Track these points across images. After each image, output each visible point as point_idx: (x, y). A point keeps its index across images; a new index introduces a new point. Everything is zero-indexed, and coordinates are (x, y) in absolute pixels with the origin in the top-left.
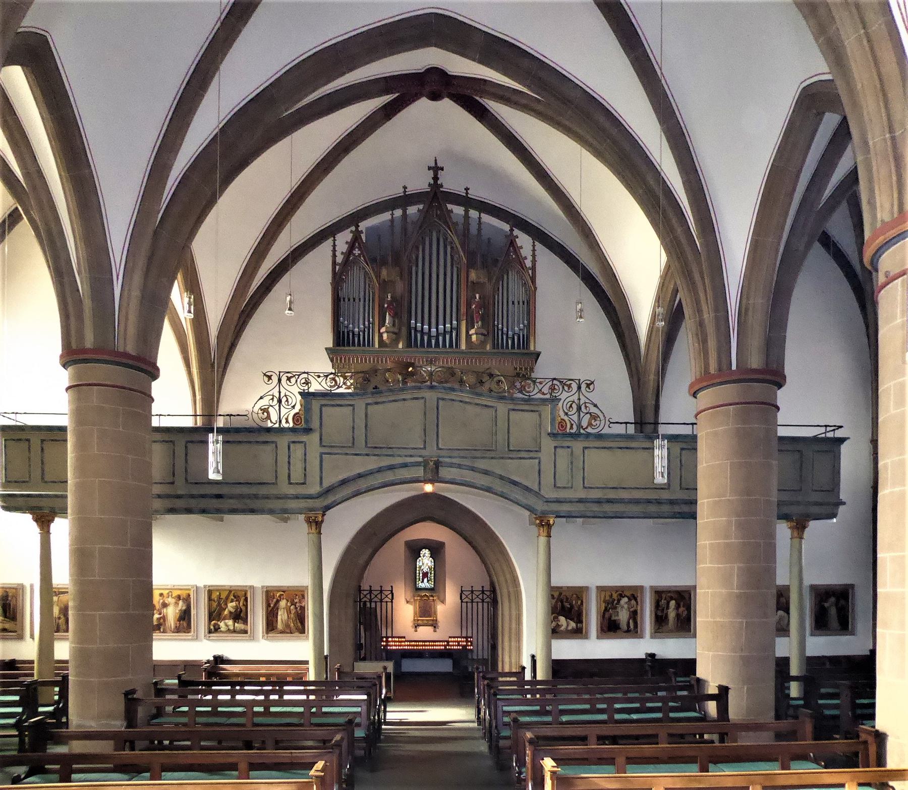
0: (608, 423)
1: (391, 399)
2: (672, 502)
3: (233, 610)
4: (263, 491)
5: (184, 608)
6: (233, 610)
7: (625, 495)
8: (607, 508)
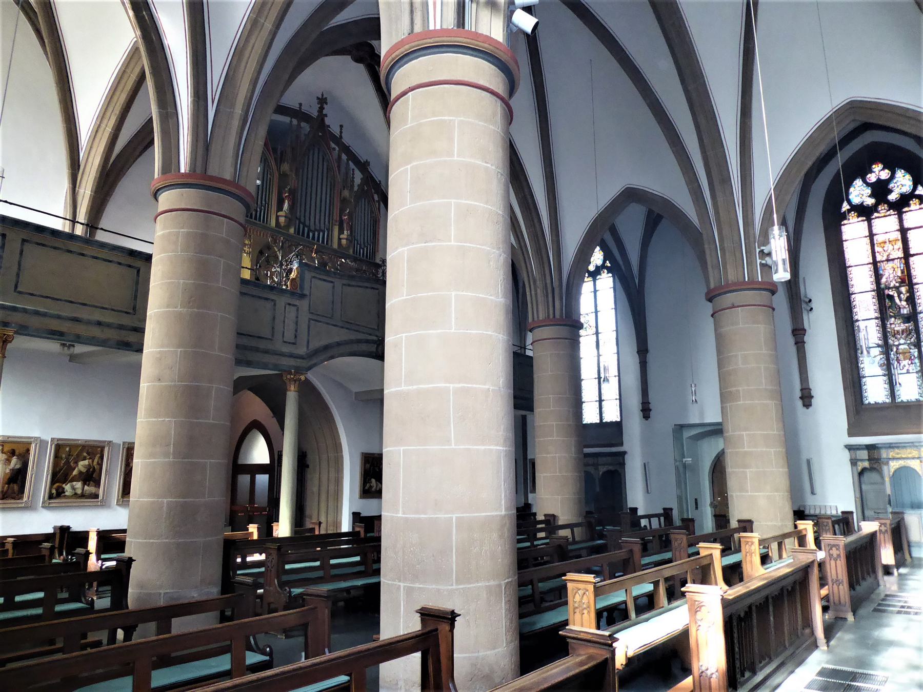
1: (321, 277)
3: (84, 470)
4: (262, 345)
5: (18, 466)
6: (84, 470)
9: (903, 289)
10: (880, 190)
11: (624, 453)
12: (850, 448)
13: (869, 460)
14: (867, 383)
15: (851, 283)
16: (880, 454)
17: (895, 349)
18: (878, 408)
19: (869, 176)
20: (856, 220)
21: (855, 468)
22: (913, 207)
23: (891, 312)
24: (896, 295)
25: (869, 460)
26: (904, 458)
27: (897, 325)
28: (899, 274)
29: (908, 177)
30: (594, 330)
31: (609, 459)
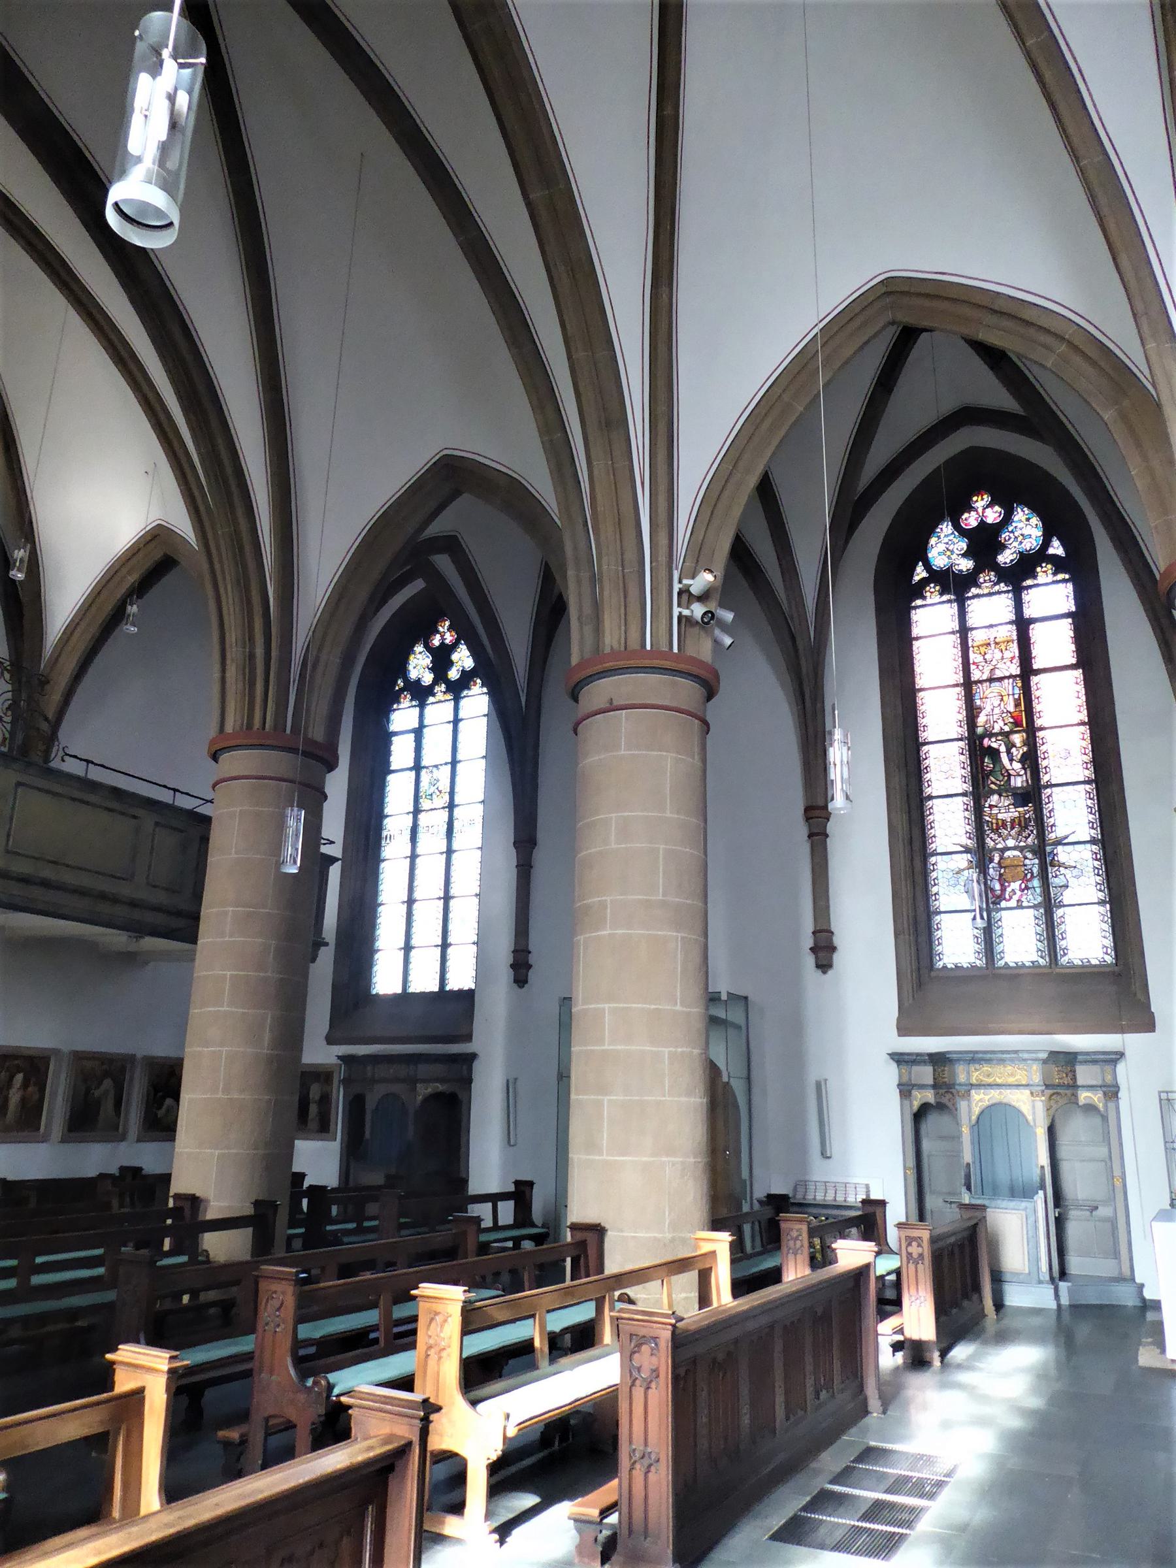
0: (61, 753)
2: (133, 904)
7: (69, 878)
8: (37, 892)
9: (1017, 739)
10: (984, 543)
11: (472, 1057)
12: (900, 1059)
13: (935, 1086)
14: (943, 926)
15: (922, 721)
16: (953, 1074)
17: (997, 859)
18: (960, 976)
19: (966, 515)
20: (937, 598)
21: (907, 1103)
22: (1042, 578)
23: (993, 783)
24: (1003, 749)
25: (935, 1086)
26: (999, 1086)
27: (1002, 809)
28: (1012, 709)
29: (1035, 520)
30: (447, 797)
31: (439, 1069)
